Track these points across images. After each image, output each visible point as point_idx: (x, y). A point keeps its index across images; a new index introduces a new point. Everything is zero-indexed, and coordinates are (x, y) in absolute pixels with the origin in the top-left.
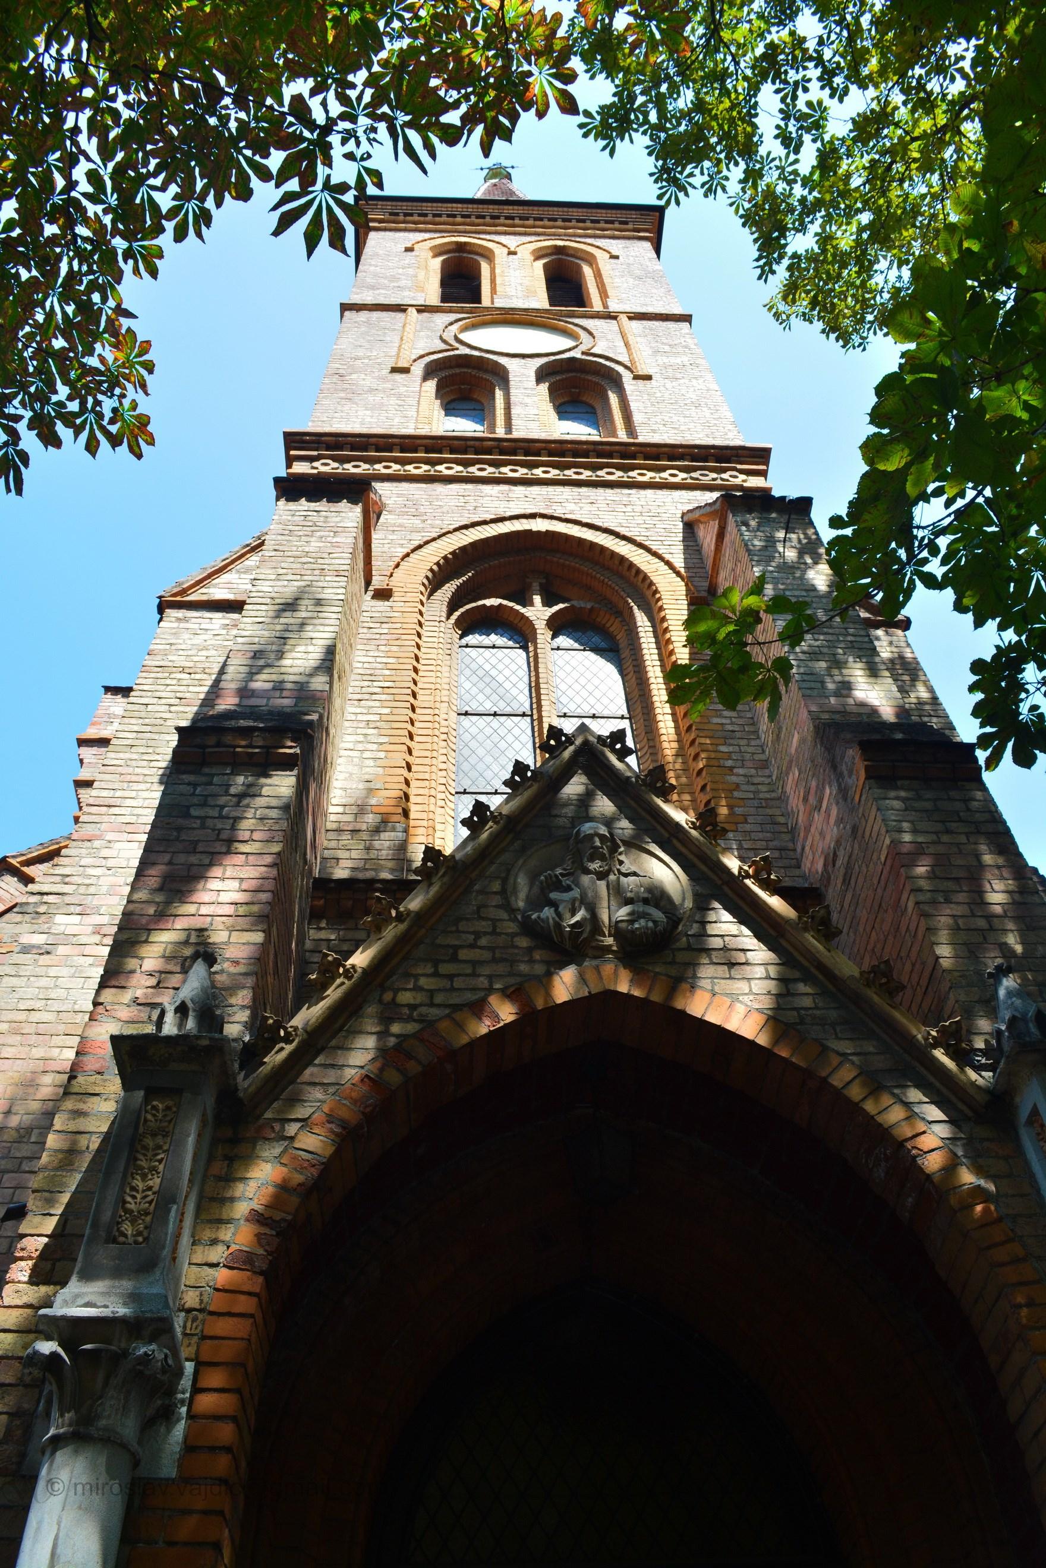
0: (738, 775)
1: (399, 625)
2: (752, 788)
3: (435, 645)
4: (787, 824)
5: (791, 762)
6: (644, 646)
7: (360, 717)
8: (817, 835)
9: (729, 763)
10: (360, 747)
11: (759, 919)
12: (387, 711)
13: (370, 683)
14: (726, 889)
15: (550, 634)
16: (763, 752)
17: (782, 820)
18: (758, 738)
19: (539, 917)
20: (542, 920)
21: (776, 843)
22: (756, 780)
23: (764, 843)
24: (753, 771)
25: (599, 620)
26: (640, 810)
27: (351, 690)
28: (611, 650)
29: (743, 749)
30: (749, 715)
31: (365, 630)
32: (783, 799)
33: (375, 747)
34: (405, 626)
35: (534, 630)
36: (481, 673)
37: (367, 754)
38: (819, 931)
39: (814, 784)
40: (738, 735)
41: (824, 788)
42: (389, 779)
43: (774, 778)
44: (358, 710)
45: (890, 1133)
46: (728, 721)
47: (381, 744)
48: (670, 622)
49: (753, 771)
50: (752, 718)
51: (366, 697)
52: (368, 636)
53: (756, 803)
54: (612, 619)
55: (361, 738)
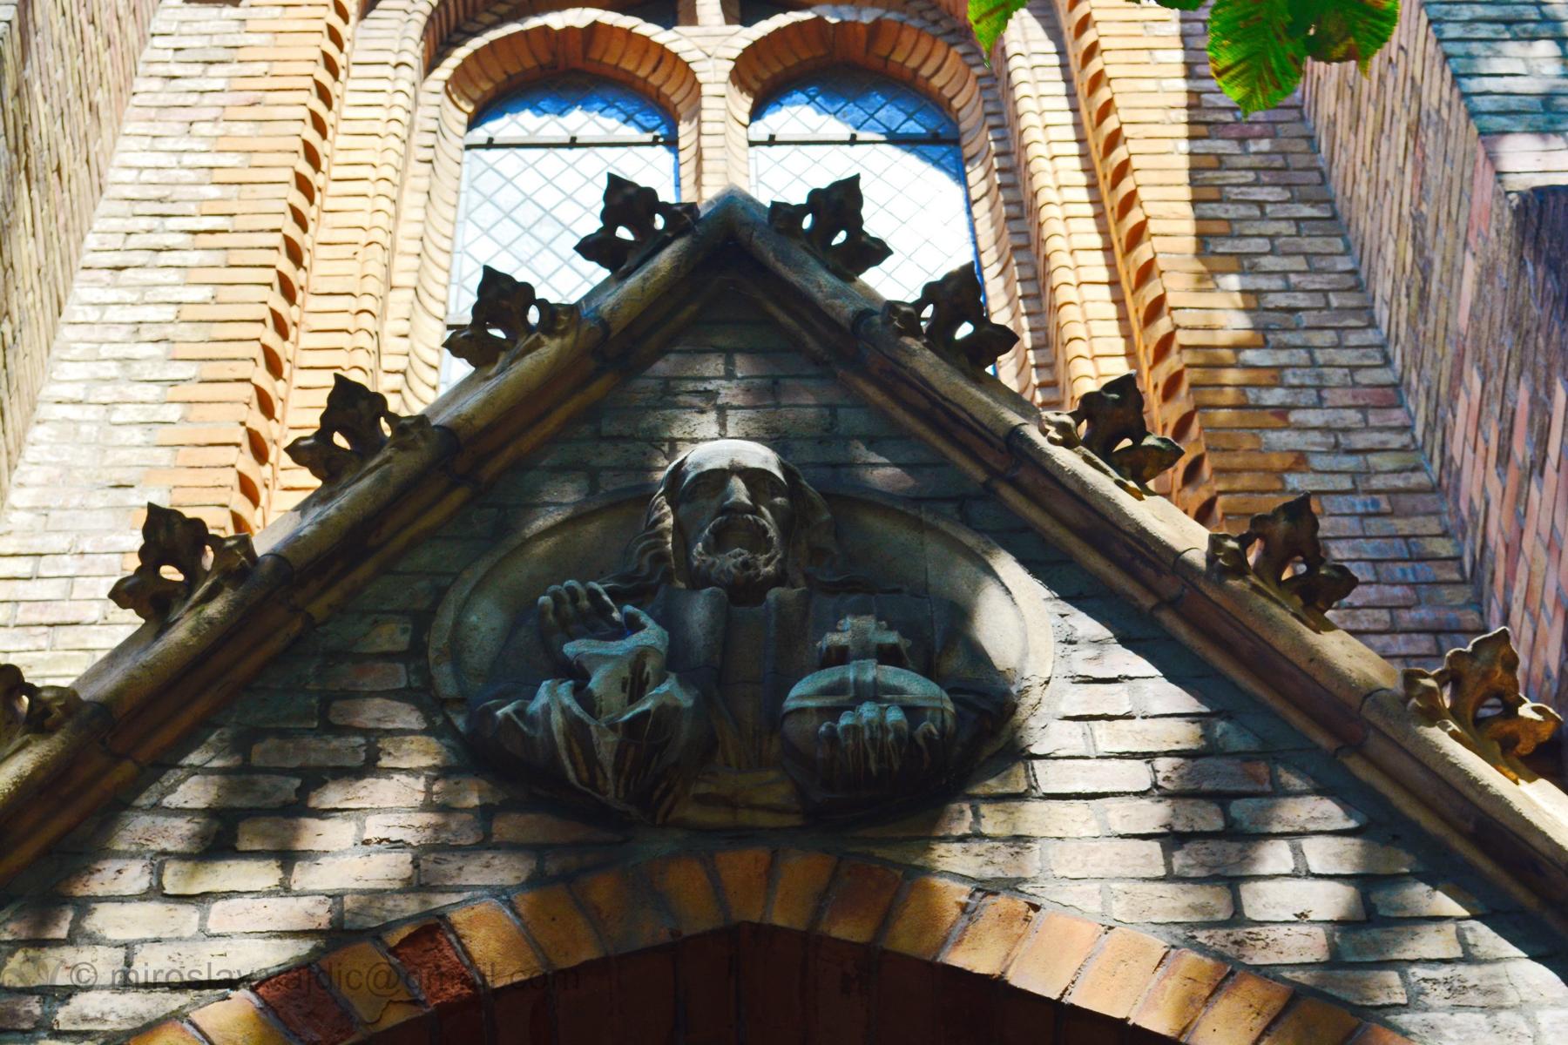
0: (1303, 428)
1: (260, 68)
2: (1349, 463)
3: (378, 127)
4: (1458, 559)
5: (1460, 356)
6: (1024, 105)
7: (114, 314)
8: (1541, 551)
9: (1275, 397)
10: (106, 393)
11: (1277, 704)
12: (204, 293)
13: (156, 222)
14: (1167, 618)
15: (743, 104)
16: (1387, 362)
17: (1443, 548)
18: (1372, 324)
19: (520, 712)
20: (531, 720)
21: (1423, 614)
22: (1360, 441)
23: (1384, 615)
24: (1352, 417)
25: (898, 57)
26: (899, 413)
27: (91, 241)
28: (933, 139)
29: (1320, 357)
30: (1344, 264)
31: (156, 84)
32: (1445, 487)
33: (153, 391)
34: (278, 68)
35: (694, 88)
36: (528, 214)
37: (122, 414)
38: (1478, 722)
39: (1523, 396)
40: (1306, 319)
41: (1550, 393)
42: (187, 478)
43: (1419, 432)
44: (112, 295)
45: (1432, 885)
46: (1277, 283)
47: (174, 382)
48: (1102, 28)
49: (1352, 417)
50: (1354, 272)
51: (139, 258)
52: (162, 99)
53: (1359, 503)
54: (924, 46)
55: (112, 370)
